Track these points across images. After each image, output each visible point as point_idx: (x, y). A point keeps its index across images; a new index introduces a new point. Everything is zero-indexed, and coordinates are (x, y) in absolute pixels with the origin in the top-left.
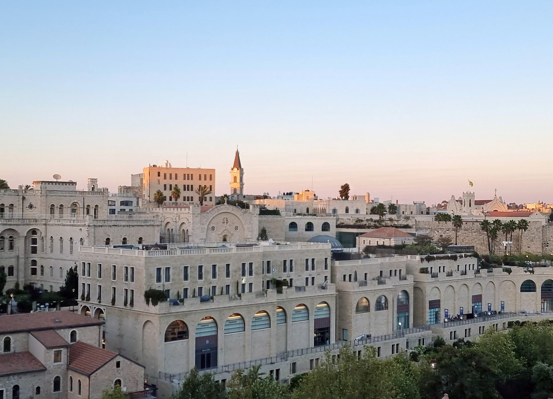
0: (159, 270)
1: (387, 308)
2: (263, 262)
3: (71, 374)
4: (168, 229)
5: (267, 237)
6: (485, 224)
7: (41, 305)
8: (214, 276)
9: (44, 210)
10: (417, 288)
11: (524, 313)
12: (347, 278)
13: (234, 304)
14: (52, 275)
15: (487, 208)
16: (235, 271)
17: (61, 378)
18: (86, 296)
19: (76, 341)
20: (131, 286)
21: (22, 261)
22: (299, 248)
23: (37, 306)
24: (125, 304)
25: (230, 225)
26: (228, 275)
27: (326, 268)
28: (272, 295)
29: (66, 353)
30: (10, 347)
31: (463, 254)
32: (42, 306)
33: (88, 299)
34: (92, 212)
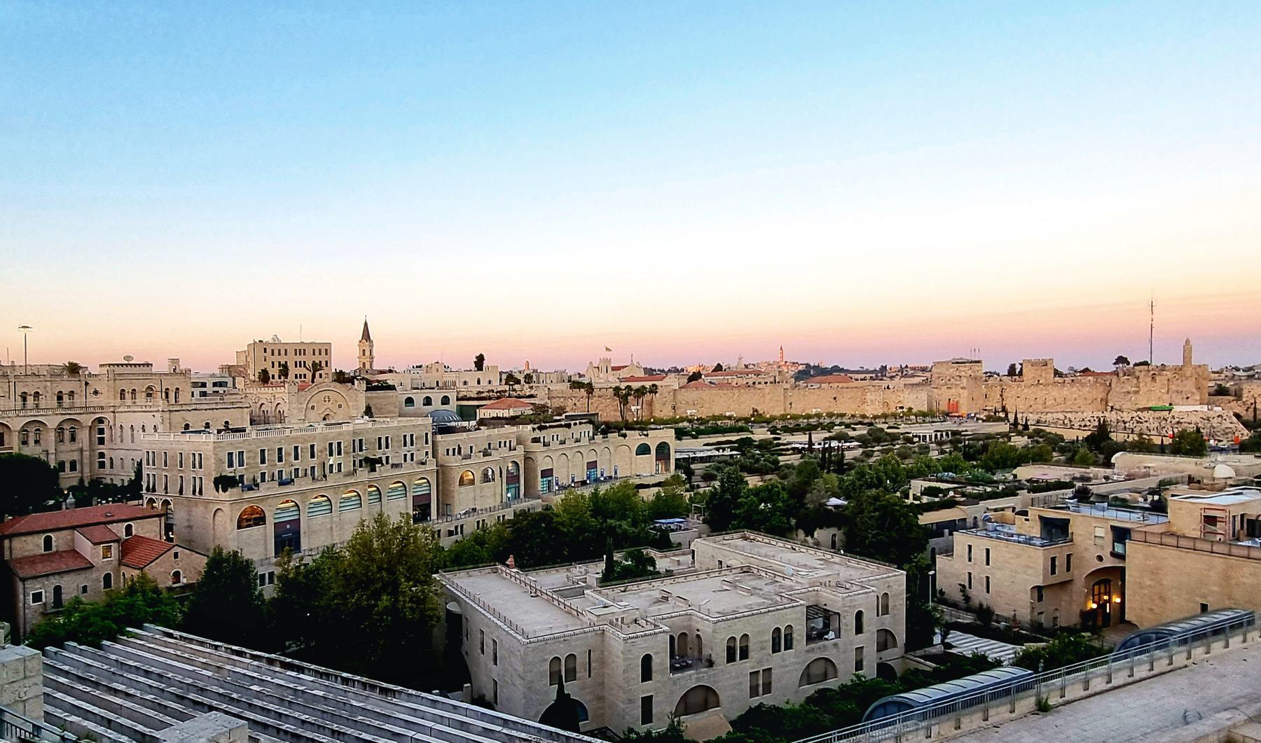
0: (230, 454)
1: (494, 480)
2: (354, 441)
3: (123, 569)
4: (263, 411)
5: (372, 414)
6: (617, 389)
7: (102, 500)
8: (296, 458)
9: (113, 396)
10: (527, 458)
11: (638, 476)
12: (451, 452)
13: (318, 485)
14: (123, 468)
15: (623, 374)
16: (321, 451)
17: (112, 575)
18: (151, 487)
19: (131, 535)
20: (201, 473)
21: (86, 454)
22: (396, 424)
23: (98, 503)
24: (194, 493)
25: (332, 404)
26: (313, 456)
27: (427, 443)
28: (364, 474)
29: (117, 548)
30: (51, 546)
31: (578, 422)
32: (104, 502)
33: (154, 490)
34: (172, 395)
